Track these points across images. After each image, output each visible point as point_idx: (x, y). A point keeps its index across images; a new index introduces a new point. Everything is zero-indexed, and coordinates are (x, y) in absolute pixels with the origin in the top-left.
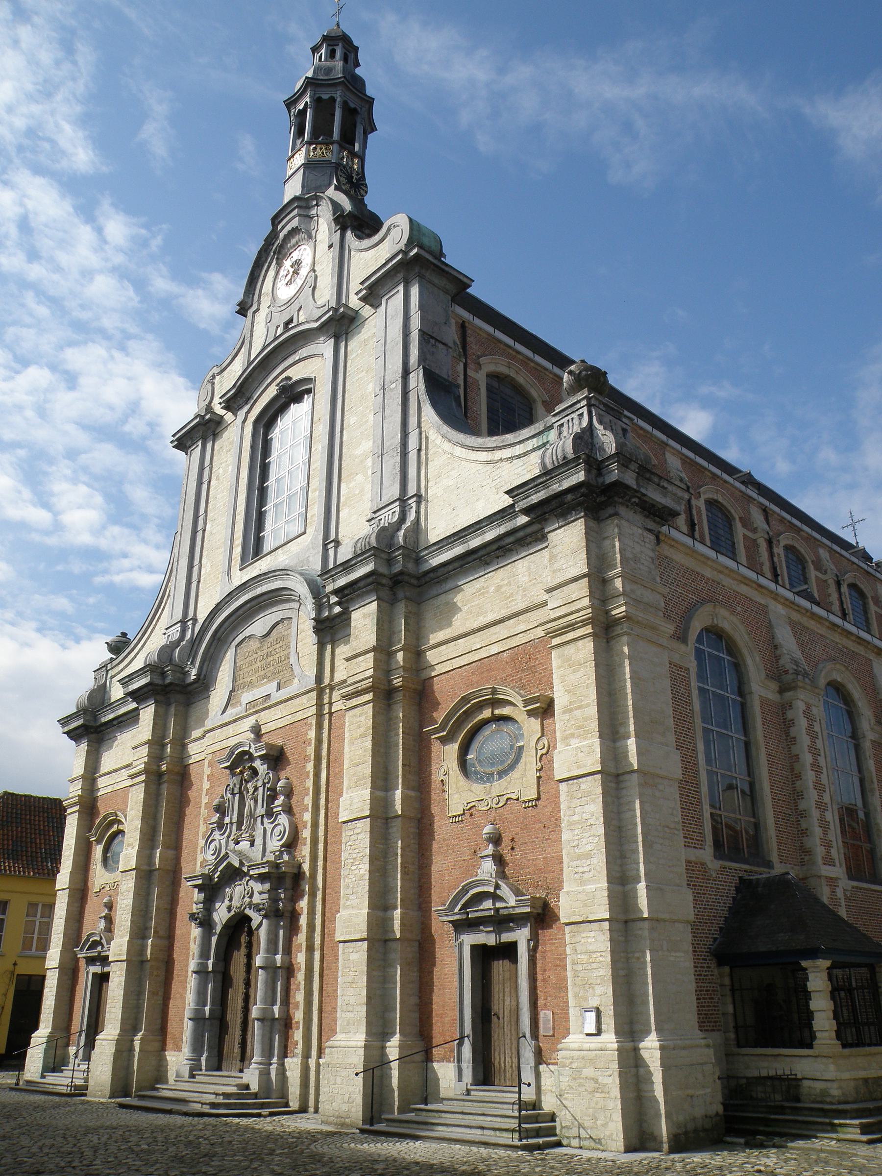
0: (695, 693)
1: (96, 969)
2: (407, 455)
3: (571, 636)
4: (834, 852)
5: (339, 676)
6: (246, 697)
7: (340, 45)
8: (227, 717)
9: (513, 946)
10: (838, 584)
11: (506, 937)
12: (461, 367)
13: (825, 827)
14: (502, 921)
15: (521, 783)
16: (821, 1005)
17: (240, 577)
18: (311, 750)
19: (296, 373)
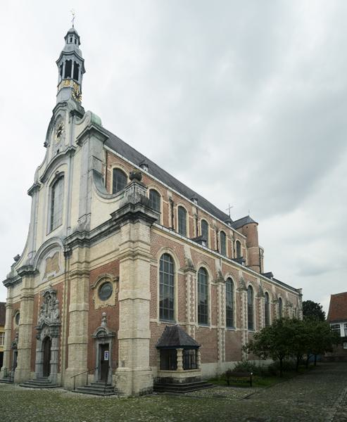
0: (158, 274)
1: (14, 351)
2: (86, 200)
3: (125, 259)
4: (194, 318)
5: (70, 269)
6: (48, 275)
7: (72, 36)
8: (43, 281)
9: (108, 344)
10: (217, 232)
11: (106, 342)
12: (105, 168)
13: (222, 311)
14: (106, 338)
15: (111, 301)
16: (180, 359)
17: (46, 239)
18: (63, 291)
19: (60, 170)
